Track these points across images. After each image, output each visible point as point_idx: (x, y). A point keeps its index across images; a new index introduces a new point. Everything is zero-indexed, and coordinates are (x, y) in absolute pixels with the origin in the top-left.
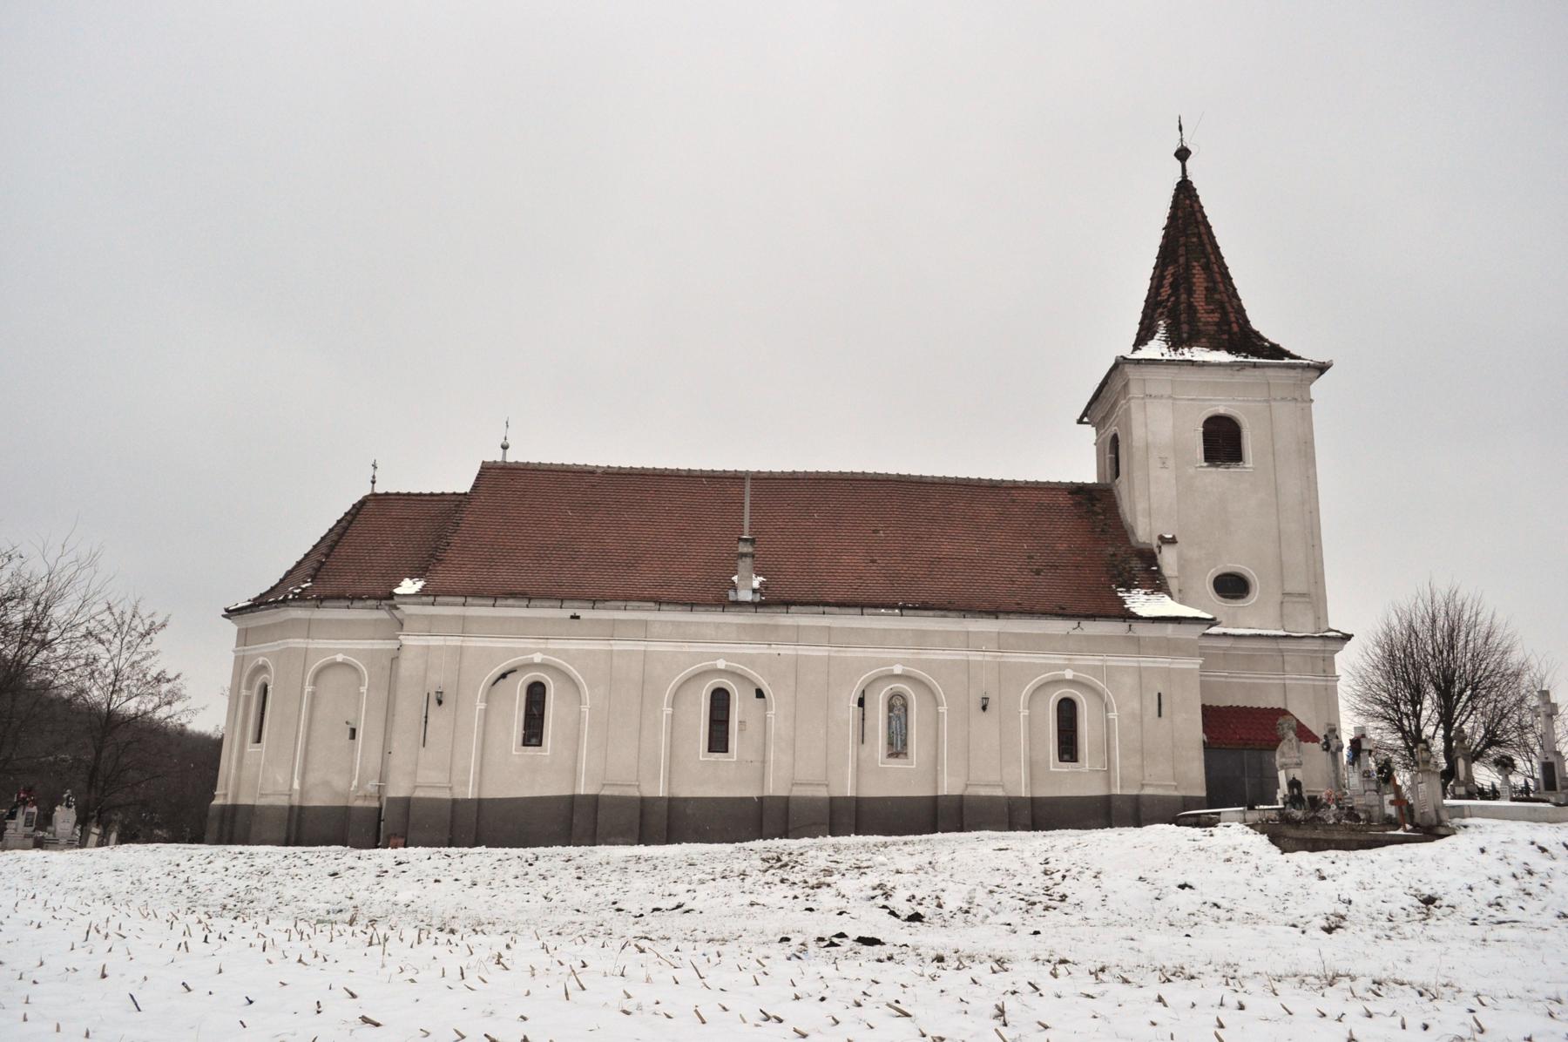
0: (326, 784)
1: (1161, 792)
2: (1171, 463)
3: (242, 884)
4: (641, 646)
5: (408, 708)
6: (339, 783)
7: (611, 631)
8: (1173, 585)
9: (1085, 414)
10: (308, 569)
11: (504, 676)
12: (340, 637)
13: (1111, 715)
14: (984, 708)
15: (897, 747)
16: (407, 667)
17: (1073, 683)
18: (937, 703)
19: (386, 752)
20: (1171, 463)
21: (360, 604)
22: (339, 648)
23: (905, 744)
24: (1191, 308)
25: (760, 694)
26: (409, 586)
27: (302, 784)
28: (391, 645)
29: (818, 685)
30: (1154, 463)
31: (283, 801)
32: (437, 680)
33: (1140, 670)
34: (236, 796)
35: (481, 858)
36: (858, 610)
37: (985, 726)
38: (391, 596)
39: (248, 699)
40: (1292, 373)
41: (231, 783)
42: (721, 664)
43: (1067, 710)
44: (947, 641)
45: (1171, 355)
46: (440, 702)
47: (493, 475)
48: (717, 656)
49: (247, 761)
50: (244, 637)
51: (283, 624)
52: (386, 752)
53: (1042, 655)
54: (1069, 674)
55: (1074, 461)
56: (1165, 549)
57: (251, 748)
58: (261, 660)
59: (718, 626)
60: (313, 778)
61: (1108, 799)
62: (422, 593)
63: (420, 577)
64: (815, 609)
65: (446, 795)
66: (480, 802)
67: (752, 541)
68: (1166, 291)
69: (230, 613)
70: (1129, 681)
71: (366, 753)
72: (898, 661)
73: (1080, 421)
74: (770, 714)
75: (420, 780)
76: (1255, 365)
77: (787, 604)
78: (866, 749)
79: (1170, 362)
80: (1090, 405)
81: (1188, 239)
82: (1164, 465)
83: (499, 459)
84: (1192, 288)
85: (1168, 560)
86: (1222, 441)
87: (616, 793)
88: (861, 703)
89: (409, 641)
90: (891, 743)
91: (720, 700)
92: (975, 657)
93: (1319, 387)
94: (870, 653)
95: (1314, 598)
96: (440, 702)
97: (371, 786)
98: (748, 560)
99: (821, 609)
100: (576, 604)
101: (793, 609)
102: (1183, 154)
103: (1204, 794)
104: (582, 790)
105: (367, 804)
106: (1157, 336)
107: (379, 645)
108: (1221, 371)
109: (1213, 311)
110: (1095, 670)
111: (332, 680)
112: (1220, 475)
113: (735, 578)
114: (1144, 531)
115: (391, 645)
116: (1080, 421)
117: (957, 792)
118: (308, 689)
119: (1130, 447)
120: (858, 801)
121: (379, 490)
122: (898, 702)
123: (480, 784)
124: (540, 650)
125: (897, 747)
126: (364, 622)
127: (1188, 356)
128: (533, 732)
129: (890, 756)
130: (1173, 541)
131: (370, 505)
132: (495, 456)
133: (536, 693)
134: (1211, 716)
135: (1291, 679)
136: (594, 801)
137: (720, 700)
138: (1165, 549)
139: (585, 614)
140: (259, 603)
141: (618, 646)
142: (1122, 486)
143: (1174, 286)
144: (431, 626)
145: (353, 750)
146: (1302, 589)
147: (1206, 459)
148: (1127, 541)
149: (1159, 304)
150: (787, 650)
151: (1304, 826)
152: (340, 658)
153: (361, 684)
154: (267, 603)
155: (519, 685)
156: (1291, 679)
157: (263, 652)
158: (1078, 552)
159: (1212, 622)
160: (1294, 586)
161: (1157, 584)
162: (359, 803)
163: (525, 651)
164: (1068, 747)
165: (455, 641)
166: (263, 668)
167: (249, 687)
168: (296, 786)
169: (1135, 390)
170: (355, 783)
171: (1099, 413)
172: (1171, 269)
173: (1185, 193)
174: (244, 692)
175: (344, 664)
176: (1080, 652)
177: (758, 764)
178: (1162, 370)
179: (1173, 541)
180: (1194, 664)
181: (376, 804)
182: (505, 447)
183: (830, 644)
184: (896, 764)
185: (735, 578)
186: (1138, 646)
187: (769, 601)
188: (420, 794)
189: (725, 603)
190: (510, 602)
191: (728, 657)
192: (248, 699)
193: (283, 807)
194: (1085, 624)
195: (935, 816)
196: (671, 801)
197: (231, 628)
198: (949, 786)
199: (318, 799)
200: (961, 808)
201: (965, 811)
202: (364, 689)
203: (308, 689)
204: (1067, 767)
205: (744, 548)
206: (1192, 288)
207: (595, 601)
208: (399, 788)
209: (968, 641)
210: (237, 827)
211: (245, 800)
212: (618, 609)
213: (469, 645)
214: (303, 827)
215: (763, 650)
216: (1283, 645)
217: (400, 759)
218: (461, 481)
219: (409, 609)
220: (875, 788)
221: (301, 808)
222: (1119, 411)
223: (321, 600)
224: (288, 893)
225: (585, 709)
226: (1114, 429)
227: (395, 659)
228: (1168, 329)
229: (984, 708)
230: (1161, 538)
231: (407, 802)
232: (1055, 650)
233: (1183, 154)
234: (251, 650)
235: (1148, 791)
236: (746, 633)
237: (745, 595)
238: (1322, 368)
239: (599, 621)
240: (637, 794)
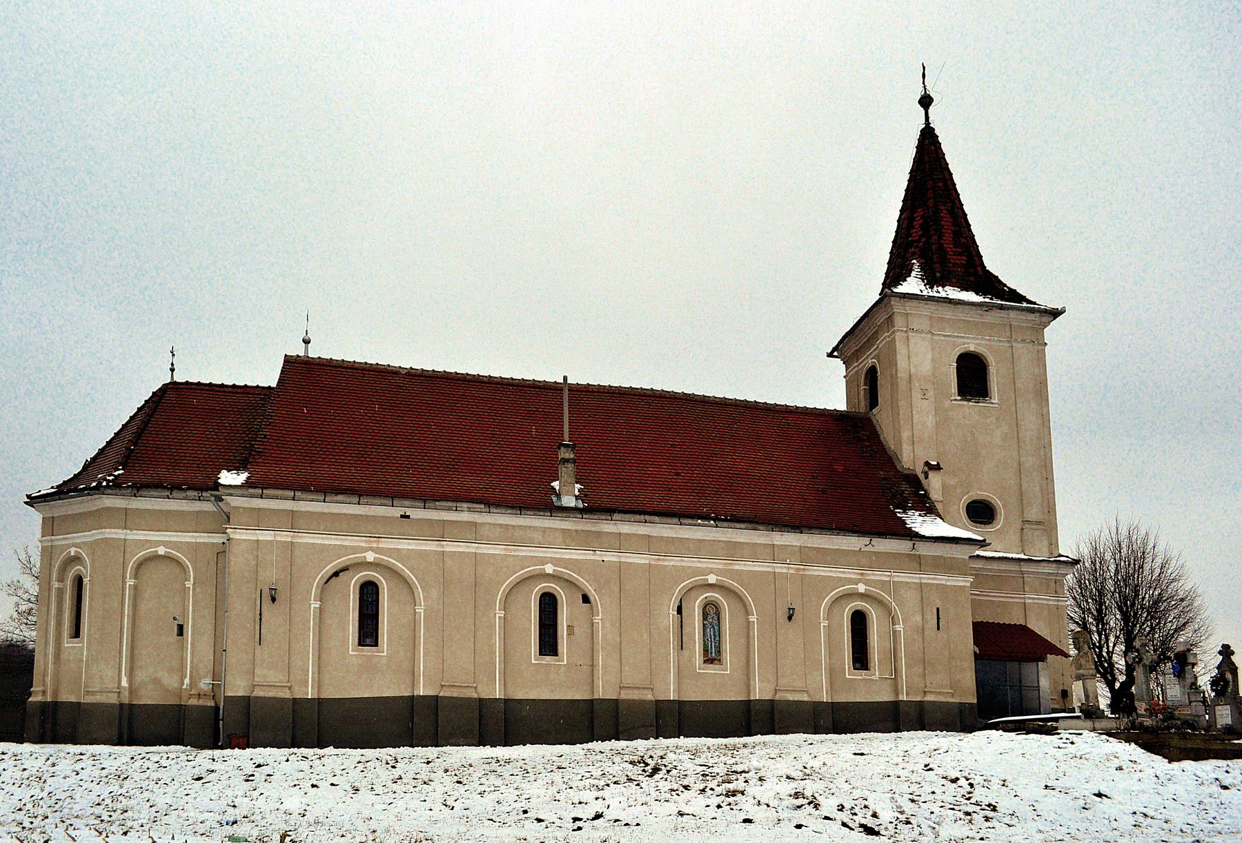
0: (157, 681)
1: (941, 699)
2: (931, 394)
3: (104, 791)
4: (472, 548)
5: (240, 606)
6: (171, 681)
7: (441, 532)
8: (939, 507)
9: (834, 350)
10: (113, 456)
11: (336, 574)
12: (160, 528)
13: (898, 628)
14: (790, 618)
15: (712, 656)
16: (238, 562)
17: (375, 565)
18: (747, 613)
19: (219, 651)
20: (931, 394)
21: (182, 494)
22: (162, 541)
23: (719, 652)
24: (941, 248)
25: (586, 599)
26: (227, 478)
27: (130, 681)
28: (217, 539)
29: (647, 589)
30: (917, 395)
31: (113, 699)
32: (271, 575)
33: (921, 586)
34: (56, 692)
35: (336, 759)
36: (675, 520)
37: (791, 633)
38: (217, 486)
39: (60, 592)
40: (1031, 317)
41: (49, 679)
42: (549, 569)
43: (859, 622)
44: (754, 552)
45: (927, 292)
46: (273, 600)
47: (299, 370)
48: (543, 561)
49: (64, 656)
50: (50, 527)
51: (100, 512)
52: (219, 651)
53: (837, 566)
54: (862, 588)
55: (828, 390)
56: (931, 474)
57: (68, 643)
58: (73, 551)
59: (545, 530)
60: (141, 676)
61: (896, 704)
62: (248, 484)
63: (245, 469)
64: (638, 517)
65: (286, 694)
66: (320, 702)
67: (573, 448)
68: (916, 232)
69: (32, 501)
70: (911, 597)
71: (197, 649)
72: (711, 571)
73: (830, 355)
74: (597, 619)
75: (628, 681)
76: (1001, 307)
77: (609, 511)
78: (686, 653)
79: (931, 298)
80: (844, 337)
81: (930, 182)
82: (924, 392)
83: (302, 354)
84: (932, 232)
85: (935, 485)
86: (972, 376)
87: (455, 695)
88: (680, 610)
89: (238, 535)
90: (706, 651)
91: (548, 604)
92: (780, 569)
93: (1053, 332)
94: (687, 562)
95: (1047, 525)
96: (273, 600)
97: (205, 684)
98: (570, 466)
99: (642, 517)
100: (407, 503)
101: (616, 516)
102: (926, 101)
103: (975, 701)
104: (600, 693)
105: (201, 702)
106: (913, 274)
107: (203, 538)
108: (973, 310)
109: (961, 254)
110: (883, 585)
111: (158, 573)
112: (971, 409)
113: (556, 484)
114: (910, 457)
115: (217, 539)
116: (830, 355)
117: (768, 696)
118: (130, 582)
119: (894, 378)
120: (680, 703)
121: (180, 378)
122: (712, 611)
123: (319, 685)
124: (371, 549)
125: (712, 656)
126: (181, 514)
127: (943, 294)
128: (368, 632)
129: (705, 662)
130: (937, 468)
131: (170, 395)
132: (298, 350)
133: (369, 593)
134: (982, 631)
135: (1031, 598)
136: (434, 702)
137: (548, 604)
138: (931, 474)
139: (417, 513)
140: (65, 490)
141: (450, 547)
142: (882, 417)
143: (925, 228)
144: (259, 520)
145: (182, 648)
146: (1040, 517)
147: (961, 392)
148: (893, 466)
149: (910, 245)
150: (611, 557)
151: (1171, 737)
152: (161, 551)
153: (187, 579)
154: (76, 490)
155: (354, 581)
156: (1031, 598)
157: (75, 542)
158: (834, 472)
159: (982, 544)
160: (1033, 513)
161: (928, 507)
162: (193, 702)
163: (356, 550)
164: (861, 659)
165: (285, 537)
166: (77, 559)
167: (61, 579)
168: (124, 683)
169: (899, 321)
170: (187, 681)
171: (63, 508)
172: (920, 212)
173: (928, 143)
174: (56, 585)
175: (167, 558)
176: (871, 568)
177: (586, 669)
178: (922, 304)
179: (937, 468)
180: (964, 582)
181: (211, 703)
182: (307, 342)
183: (650, 551)
184: (712, 670)
185: (556, 484)
186: (919, 563)
187: (592, 508)
188: (259, 693)
189: (547, 505)
190: (339, 497)
191: (555, 562)
192: (60, 592)
193: (112, 706)
194: (876, 541)
195: (749, 720)
196: (507, 701)
197: (35, 517)
198: (760, 691)
199: (148, 698)
200: (772, 712)
201: (621, 707)
202: (189, 584)
203: (130, 582)
204: (861, 675)
205: (565, 454)
206: (932, 232)
207: (426, 498)
208: (237, 687)
209: (774, 554)
210: (63, 725)
211: (67, 697)
212: (449, 509)
213: (319, 537)
214: (136, 725)
215: (588, 556)
216: (1025, 568)
217: (236, 657)
218: (268, 376)
219: (235, 501)
220: (694, 694)
221: (131, 706)
222: (881, 342)
223: (139, 488)
224: (161, 801)
225: (420, 610)
226: (870, 362)
227: (222, 552)
228: (922, 268)
229: (790, 618)
230: (927, 464)
231: (246, 702)
232: (848, 565)
233: (926, 101)
234: (59, 540)
235: (930, 698)
236: (570, 539)
237: (569, 501)
238: (1055, 314)
239: (430, 521)
240: (476, 696)
